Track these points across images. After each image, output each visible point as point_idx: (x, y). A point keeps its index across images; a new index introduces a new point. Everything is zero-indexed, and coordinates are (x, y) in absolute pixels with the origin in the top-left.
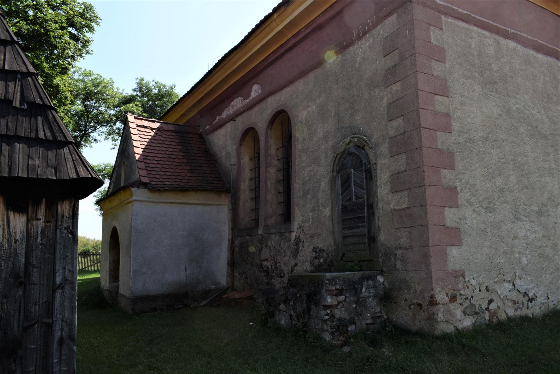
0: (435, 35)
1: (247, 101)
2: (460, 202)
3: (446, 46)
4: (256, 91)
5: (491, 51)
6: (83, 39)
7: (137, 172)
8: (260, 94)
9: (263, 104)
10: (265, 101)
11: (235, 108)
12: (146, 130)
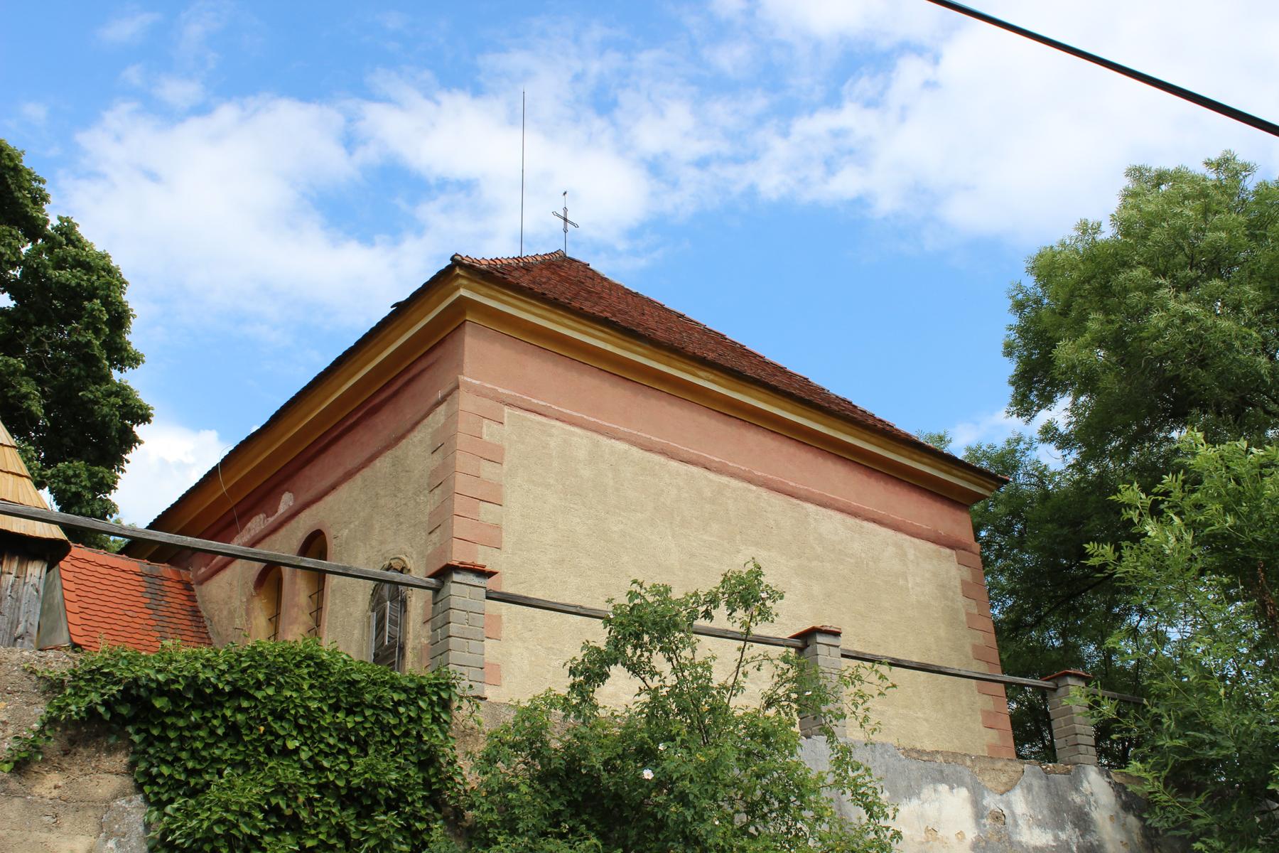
0: (489, 431)
1: (271, 520)
2: (504, 634)
3: (506, 445)
4: (286, 502)
5: (582, 454)
6: (1023, 568)
7: (65, 628)
8: (290, 507)
9: (293, 523)
10: (297, 519)
11: (253, 533)
12: (87, 566)
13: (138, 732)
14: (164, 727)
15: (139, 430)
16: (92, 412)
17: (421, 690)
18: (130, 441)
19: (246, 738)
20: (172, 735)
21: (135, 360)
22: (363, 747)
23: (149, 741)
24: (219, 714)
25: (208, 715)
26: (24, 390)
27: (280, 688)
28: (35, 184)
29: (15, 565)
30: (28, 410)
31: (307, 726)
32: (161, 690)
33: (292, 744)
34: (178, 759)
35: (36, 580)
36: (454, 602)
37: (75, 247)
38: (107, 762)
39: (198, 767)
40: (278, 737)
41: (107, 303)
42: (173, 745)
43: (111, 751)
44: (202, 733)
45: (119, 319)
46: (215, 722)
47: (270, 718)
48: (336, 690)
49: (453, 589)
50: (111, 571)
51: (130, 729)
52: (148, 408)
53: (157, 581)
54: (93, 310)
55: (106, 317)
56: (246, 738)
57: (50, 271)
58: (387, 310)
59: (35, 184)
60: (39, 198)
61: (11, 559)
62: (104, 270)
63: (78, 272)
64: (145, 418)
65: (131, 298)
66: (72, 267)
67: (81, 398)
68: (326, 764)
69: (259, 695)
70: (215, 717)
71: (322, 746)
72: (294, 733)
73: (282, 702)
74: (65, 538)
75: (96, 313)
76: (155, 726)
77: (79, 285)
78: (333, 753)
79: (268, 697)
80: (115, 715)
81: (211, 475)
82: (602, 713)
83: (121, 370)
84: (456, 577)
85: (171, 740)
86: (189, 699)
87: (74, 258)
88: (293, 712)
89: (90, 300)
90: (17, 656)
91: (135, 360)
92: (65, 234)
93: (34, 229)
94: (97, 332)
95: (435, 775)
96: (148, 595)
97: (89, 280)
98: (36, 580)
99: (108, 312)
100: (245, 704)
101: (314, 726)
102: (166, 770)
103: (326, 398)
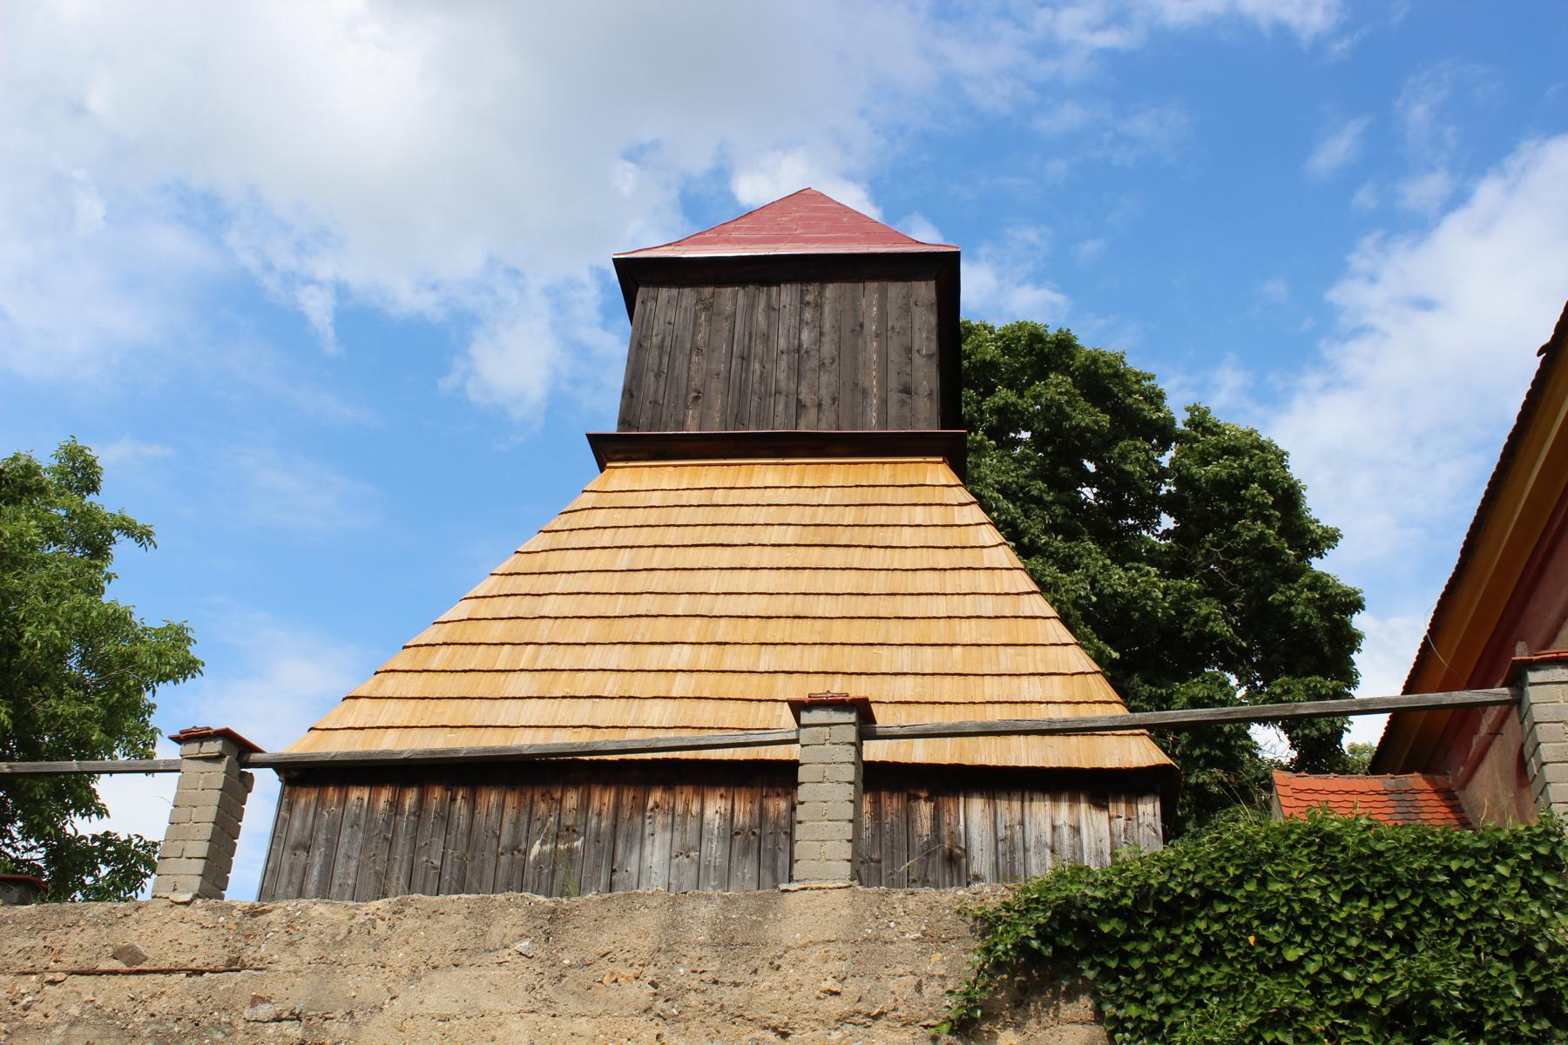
13: (1091, 968)
14: (1125, 957)
15: (1358, 621)
16: (1291, 616)
17: (1503, 851)
18: (1352, 640)
19: (1230, 955)
20: (1136, 964)
21: (1332, 537)
22: (1407, 945)
23: (1107, 975)
24: (1192, 928)
25: (1178, 931)
26: (1204, 612)
27: (1262, 883)
28: (1146, 383)
29: (1122, 806)
30: (1214, 635)
31: (1308, 921)
32: (1109, 909)
33: (1291, 955)
34: (1149, 995)
35: (1150, 819)
36: (1538, 713)
37: (1214, 434)
38: (1067, 1010)
39: (1173, 1001)
40: (1270, 946)
41: (1268, 484)
42: (1139, 977)
43: (1071, 996)
44: (1174, 957)
45: (1289, 497)
46: (1187, 940)
47: (1256, 923)
48: (1352, 870)
49: (1533, 694)
50: (1347, 797)
51: (1084, 965)
52: (1356, 593)
53: (1408, 797)
54: (1254, 497)
55: (1270, 500)
56: (1230, 955)
57: (1194, 470)
58: (1536, 363)
59: (1146, 383)
60: (1155, 398)
61: (1116, 800)
62: (1252, 447)
63: (1226, 460)
64: (1355, 605)
65: (1297, 469)
66: (1219, 458)
67: (1271, 603)
68: (1349, 975)
69: (1238, 894)
70: (1187, 933)
71: (1341, 951)
72: (1298, 939)
73: (1268, 900)
74: (1168, 761)
75: (1260, 499)
76: (1112, 957)
77: (1231, 475)
78: (1361, 958)
79: (1249, 896)
80: (1060, 952)
81: (1425, 649)
82: (148, 695)
83: (1320, 555)
84: (1533, 677)
85: (1136, 972)
86: (1150, 915)
87: (1215, 446)
88: (1284, 910)
89: (1247, 488)
90: (950, 896)
91: (1332, 537)
92: (1200, 424)
93: (1164, 433)
94: (1267, 521)
95: (1536, 971)
96: (1398, 817)
97: (1241, 466)
98: (1150, 819)
99: (1271, 493)
100: (1223, 909)
101: (1323, 925)
102: (1133, 1011)
103: (1516, 503)
